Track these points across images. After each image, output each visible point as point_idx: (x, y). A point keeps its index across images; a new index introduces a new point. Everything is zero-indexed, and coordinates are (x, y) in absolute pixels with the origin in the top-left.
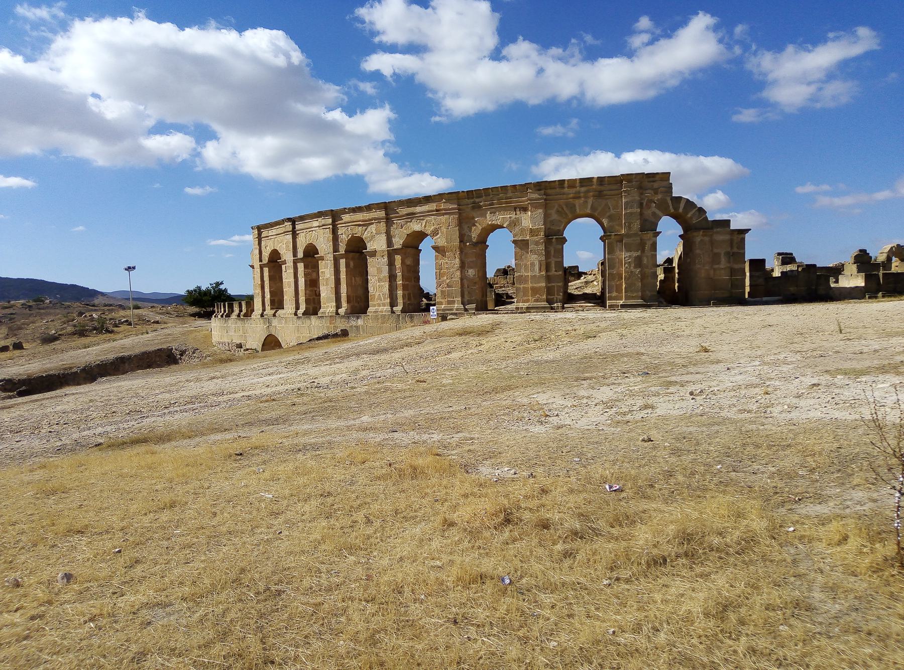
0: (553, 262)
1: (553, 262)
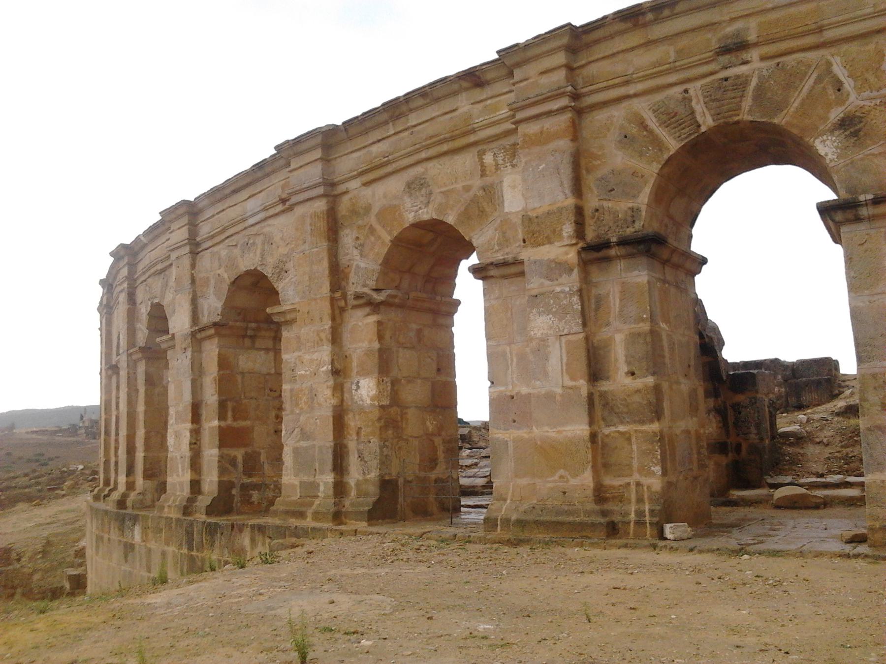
0: (619, 338)
1: (619, 338)
